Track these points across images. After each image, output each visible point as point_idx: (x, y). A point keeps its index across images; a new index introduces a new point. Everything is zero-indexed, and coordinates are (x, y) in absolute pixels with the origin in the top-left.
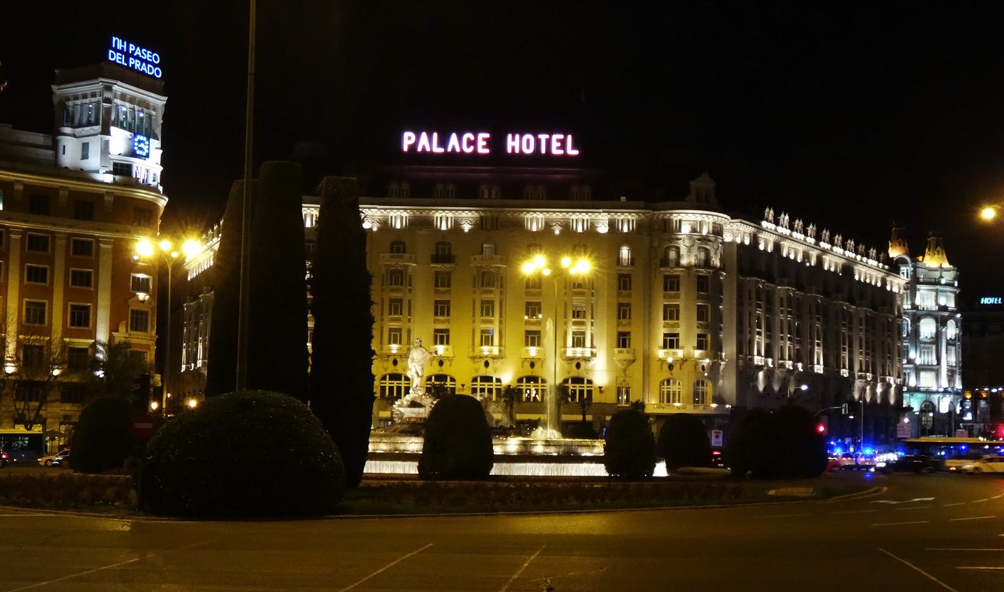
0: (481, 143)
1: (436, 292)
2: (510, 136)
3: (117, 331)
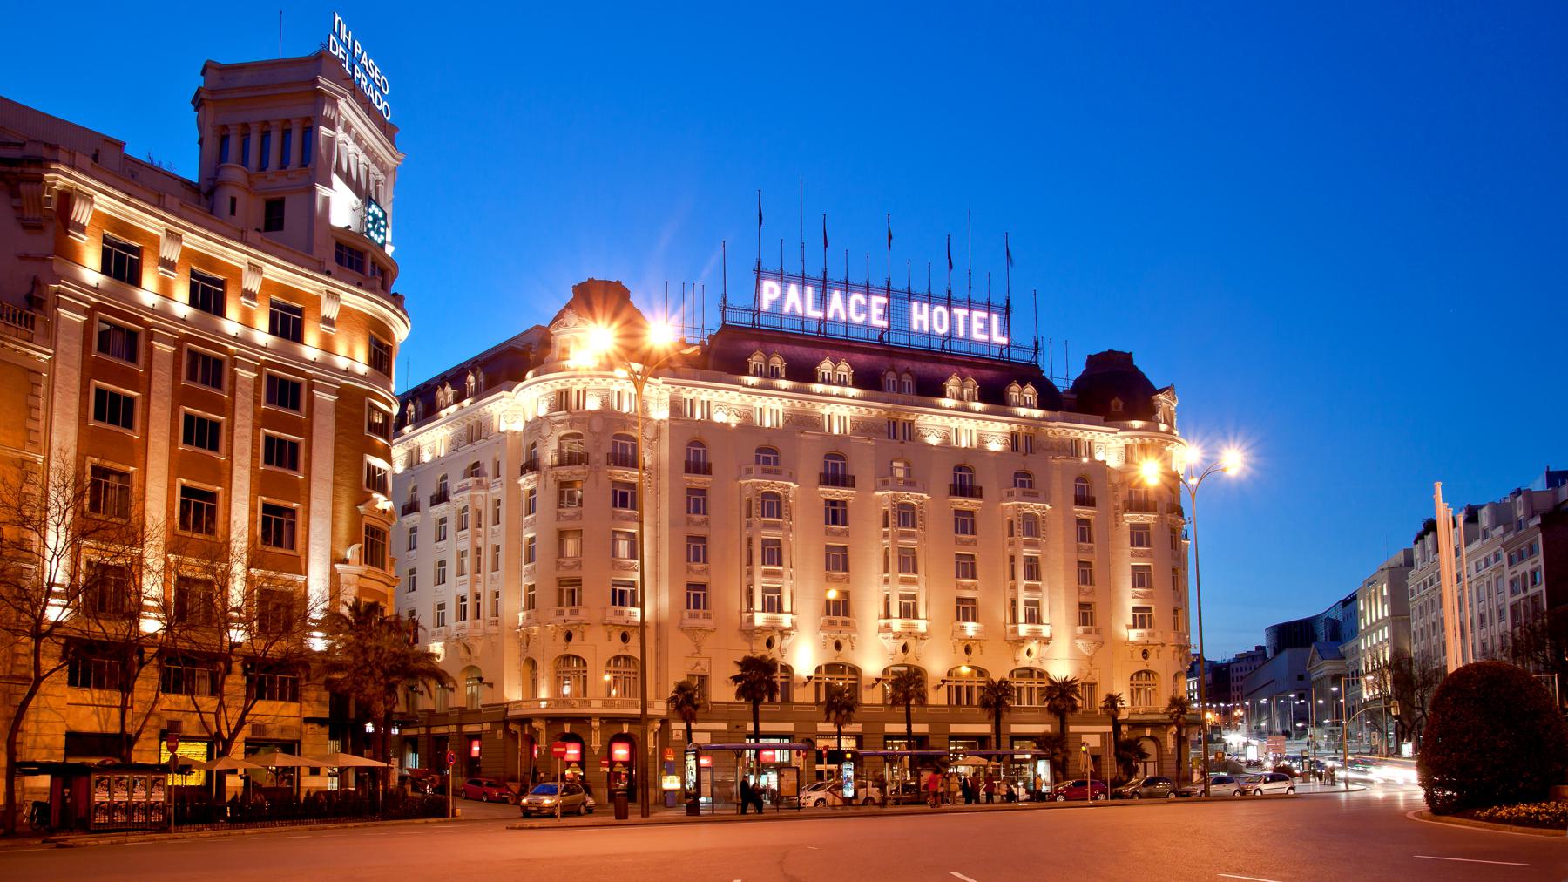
0: (876, 311)
1: (827, 532)
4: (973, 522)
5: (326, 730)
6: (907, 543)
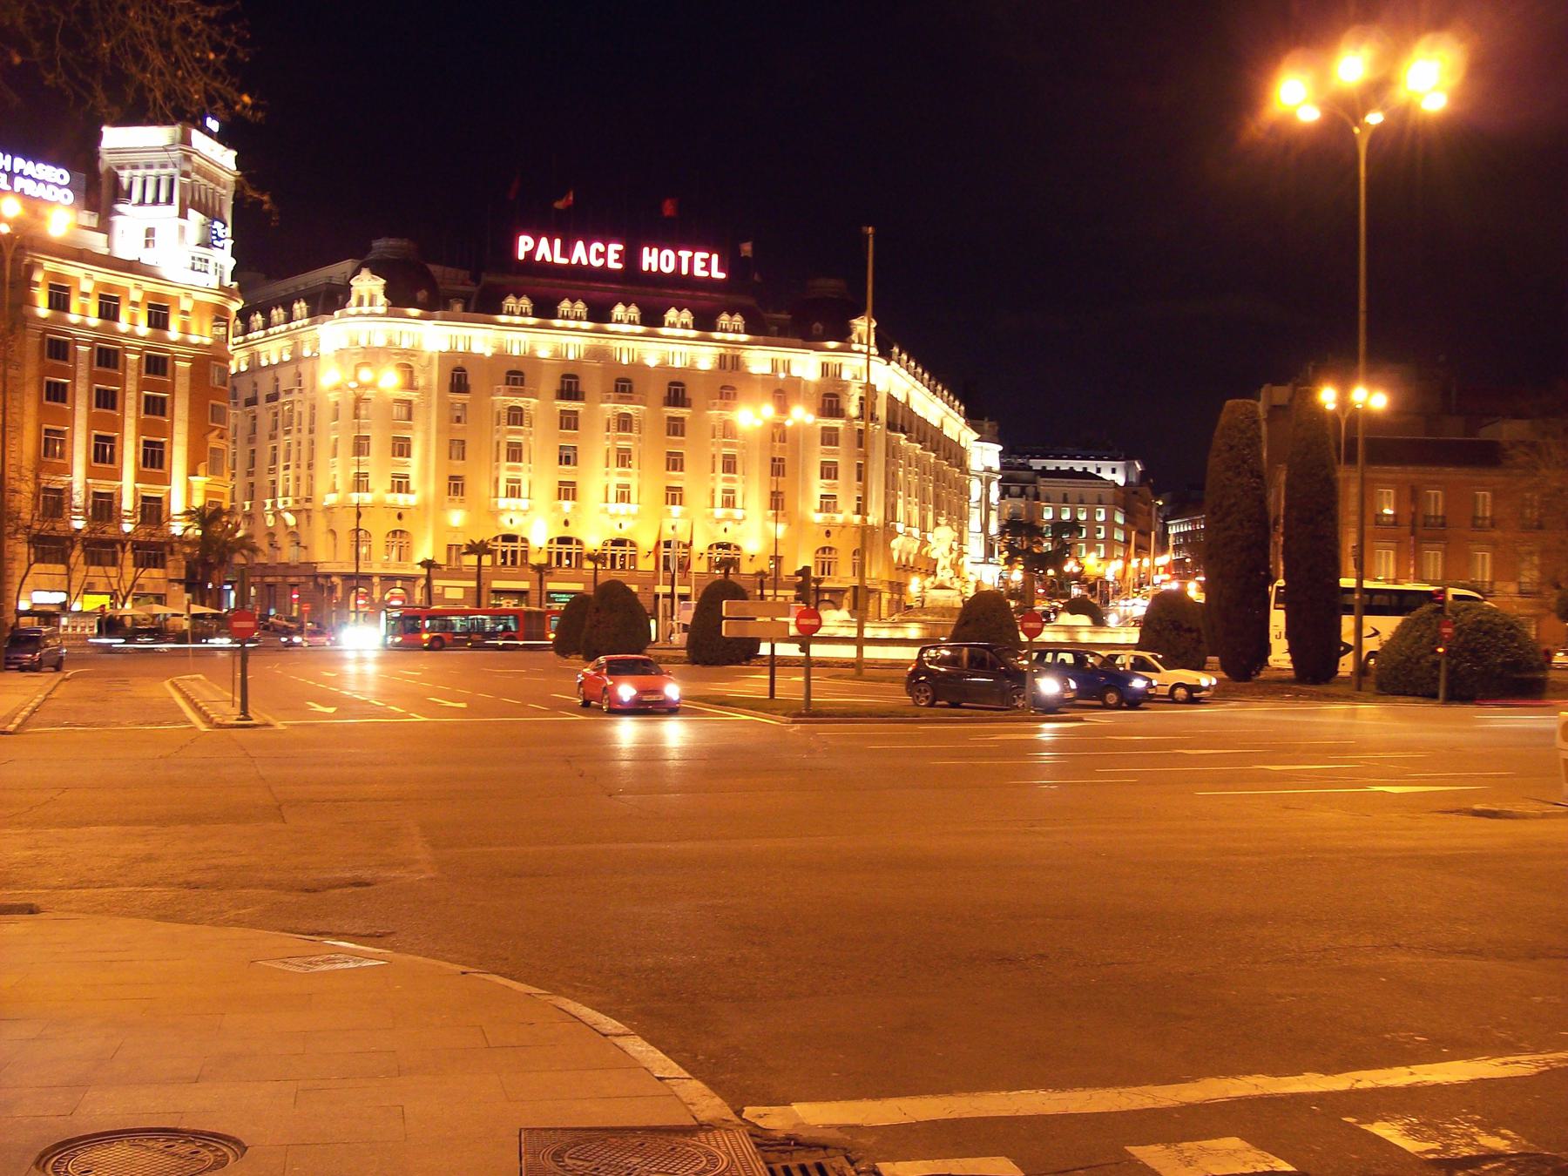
0: (612, 256)
2: (646, 250)
3: (195, 475)
4: (683, 426)
5: (182, 587)
6: (623, 444)
